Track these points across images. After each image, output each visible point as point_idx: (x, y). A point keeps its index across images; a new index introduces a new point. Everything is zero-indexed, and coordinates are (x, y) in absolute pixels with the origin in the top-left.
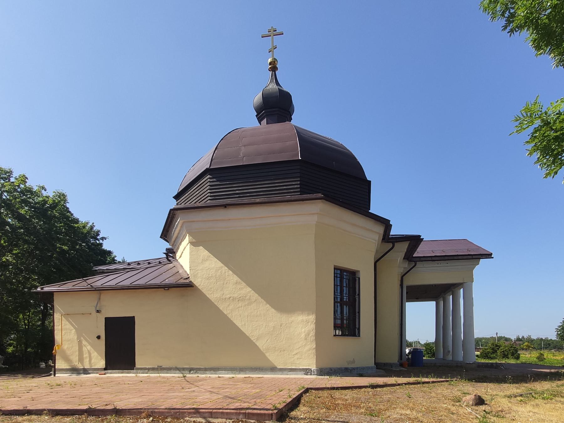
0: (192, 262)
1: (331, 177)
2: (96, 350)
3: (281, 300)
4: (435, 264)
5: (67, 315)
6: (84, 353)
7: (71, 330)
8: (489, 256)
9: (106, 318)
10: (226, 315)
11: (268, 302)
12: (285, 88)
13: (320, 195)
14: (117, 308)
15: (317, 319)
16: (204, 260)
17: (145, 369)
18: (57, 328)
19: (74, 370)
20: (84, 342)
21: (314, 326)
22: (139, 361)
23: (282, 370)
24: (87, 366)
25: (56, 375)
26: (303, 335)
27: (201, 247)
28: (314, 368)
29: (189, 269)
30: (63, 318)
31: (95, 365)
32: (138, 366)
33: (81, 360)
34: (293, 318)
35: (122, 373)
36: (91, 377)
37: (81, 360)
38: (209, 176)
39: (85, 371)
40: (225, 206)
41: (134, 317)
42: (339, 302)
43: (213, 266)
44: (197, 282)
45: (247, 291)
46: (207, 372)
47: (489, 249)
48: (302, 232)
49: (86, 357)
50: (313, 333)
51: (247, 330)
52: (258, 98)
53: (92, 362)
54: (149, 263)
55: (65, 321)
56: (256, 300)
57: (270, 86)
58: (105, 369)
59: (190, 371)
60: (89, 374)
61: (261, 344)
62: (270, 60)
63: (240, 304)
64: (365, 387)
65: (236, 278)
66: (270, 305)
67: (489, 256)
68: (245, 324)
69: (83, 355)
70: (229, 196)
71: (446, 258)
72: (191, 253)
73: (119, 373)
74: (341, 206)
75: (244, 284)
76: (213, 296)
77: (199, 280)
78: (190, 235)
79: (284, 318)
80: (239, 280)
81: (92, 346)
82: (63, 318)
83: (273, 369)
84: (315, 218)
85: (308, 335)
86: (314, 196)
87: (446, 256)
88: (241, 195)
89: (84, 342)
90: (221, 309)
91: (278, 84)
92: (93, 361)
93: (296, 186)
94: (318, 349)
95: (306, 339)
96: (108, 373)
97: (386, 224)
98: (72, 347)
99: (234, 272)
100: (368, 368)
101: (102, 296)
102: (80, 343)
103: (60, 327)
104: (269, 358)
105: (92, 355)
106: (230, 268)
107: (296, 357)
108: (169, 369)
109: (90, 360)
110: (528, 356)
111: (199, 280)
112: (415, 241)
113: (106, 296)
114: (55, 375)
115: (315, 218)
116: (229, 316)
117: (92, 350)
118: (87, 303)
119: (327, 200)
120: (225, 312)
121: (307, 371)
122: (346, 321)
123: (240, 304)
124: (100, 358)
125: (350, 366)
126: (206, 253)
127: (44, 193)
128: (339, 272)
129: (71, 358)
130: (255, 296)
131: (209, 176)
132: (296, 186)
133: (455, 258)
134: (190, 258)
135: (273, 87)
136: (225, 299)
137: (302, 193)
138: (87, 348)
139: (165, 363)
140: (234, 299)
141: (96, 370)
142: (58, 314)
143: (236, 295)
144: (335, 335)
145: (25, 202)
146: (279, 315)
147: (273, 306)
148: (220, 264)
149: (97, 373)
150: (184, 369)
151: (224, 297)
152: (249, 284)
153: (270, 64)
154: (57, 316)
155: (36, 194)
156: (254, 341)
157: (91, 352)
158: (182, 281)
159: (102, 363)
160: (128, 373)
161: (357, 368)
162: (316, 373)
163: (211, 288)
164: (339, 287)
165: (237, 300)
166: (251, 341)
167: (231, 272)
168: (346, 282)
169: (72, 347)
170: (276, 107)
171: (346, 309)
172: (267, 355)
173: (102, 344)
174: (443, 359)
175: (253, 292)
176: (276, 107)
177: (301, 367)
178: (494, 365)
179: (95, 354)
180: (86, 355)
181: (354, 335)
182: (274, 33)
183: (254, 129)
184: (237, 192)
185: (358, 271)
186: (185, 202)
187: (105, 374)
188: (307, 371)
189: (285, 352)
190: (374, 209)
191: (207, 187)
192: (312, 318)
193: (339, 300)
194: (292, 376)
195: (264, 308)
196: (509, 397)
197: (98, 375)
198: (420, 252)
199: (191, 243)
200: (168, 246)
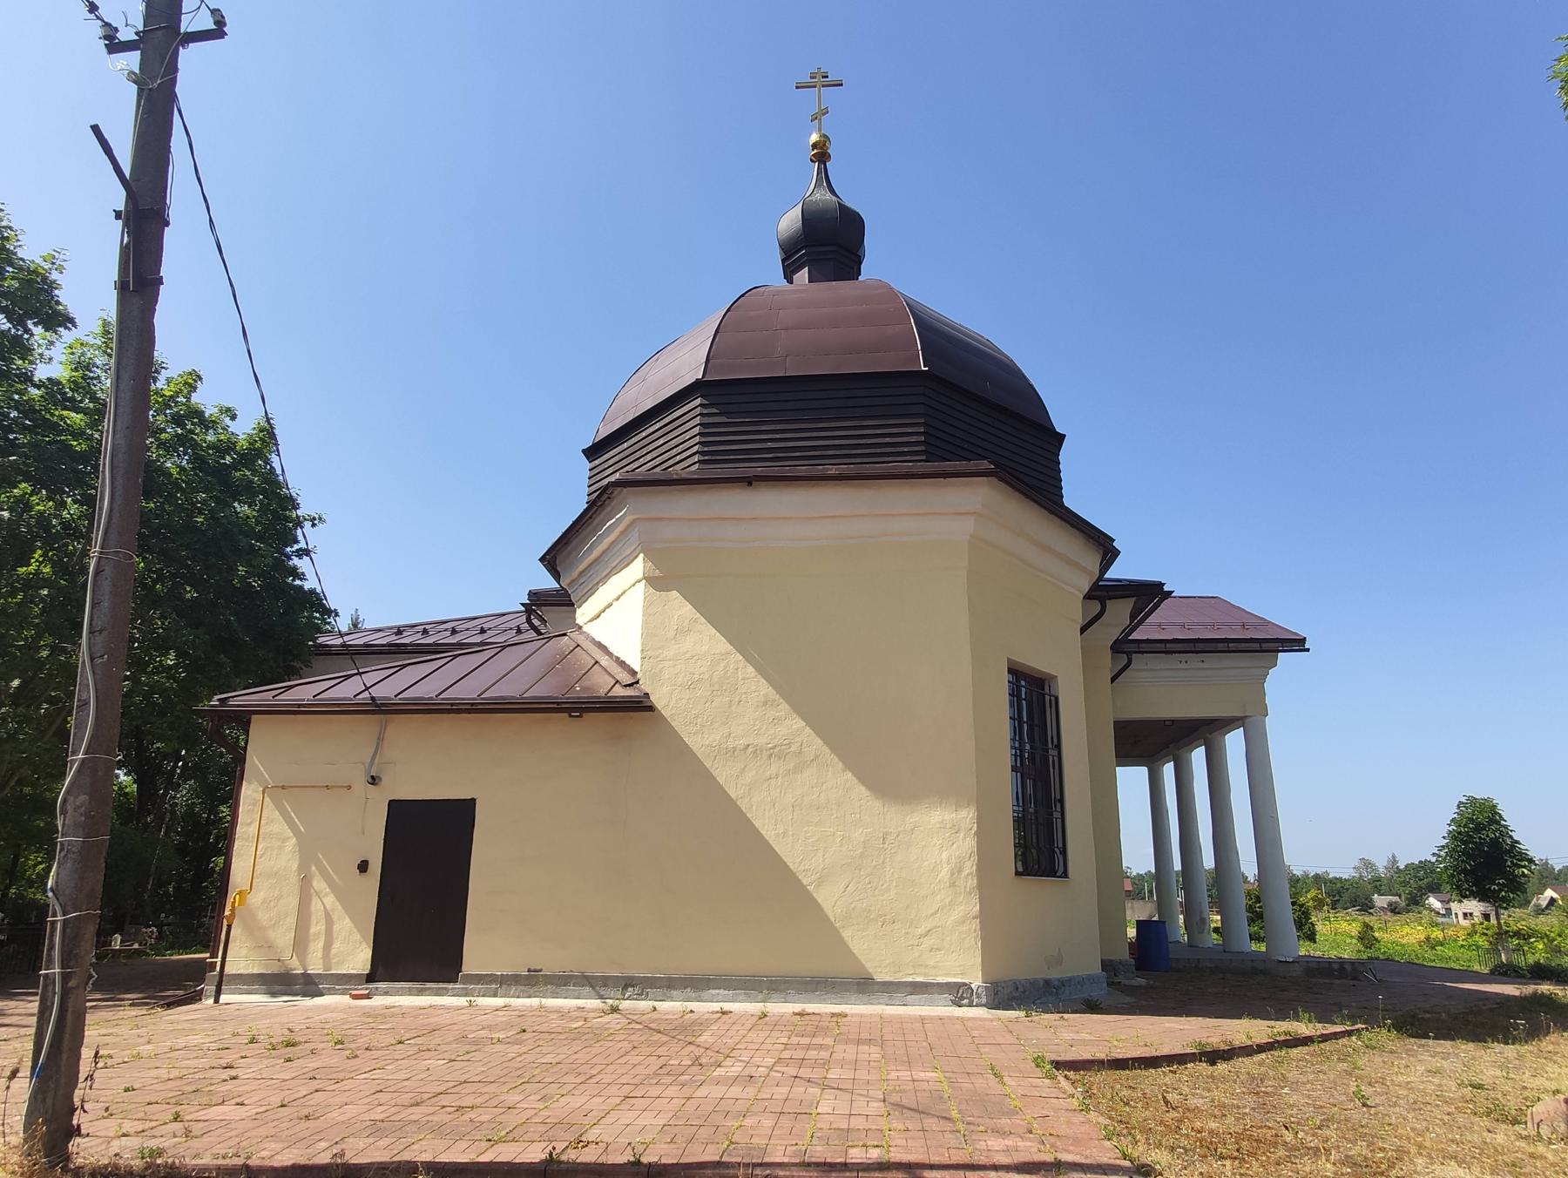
0: (649, 635)
1: (967, 419)
2: (349, 909)
4: (1172, 661)
5: (279, 790)
6: (314, 919)
7: (284, 841)
8: (1297, 644)
9: (392, 803)
10: (733, 803)
11: (849, 765)
12: (850, 203)
13: (985, 465)
14: (427, 770)
15: (980, 820)
16: (681, 632)
17: (491, 979)
18: (245, 831)
19: (282, 983)
21: (974, 843)
22: (477, 953)
24: (315, 968)
25: (224, 998)
26: (944, 873)
28: (976, 981)
29: (639, 655)
30: (267, 799)
32: (470, 965)
33: (300, 943)
34: (915, 818)
35: (420, 992)
36: (325, 1008)
37: (300, 943)
38: (698, 401)
39: (309, 985)
40: (749, 481)
41: (470, 804)
43: (705, 648)
45: (794, 726)
46: (675, 993)
47: (1296, 627)
48: (915, 557)
50: (970, 867)
51: (789, 852)
52: (790, 221)
53: (333, 952)
54: (483, 631)
55: (271, 811)
56: (817, 757)
57: (818, 196)
58: (370, 978)
59: (625, 988)
60: (322, 995)
61: (830, 899)
62: (814, 138)
63: (773, 770)
64: (1180, 1059)
65: (764, 689)
66: (854, 774)
67: (1297, 644)
69: (308, 928)
70: (749, 456)
71: (1200, 646)
73: (410, 992)
74: (1027, 496)
75: (785, 706)
76: (700, 741)
77: (666, 689)
78: (649, 556)
79: (893, 818)
81: (340, 897)
82: (267, 799)
83: (865, 986)
84: (969, 525)
85: (960, 871)
86: (972, 465)
87: (1199, 640)
88: (780, 455)
89: (319, 884)
92: (337, 947)
93: (914, 439)
94: (985, 917)
95: (953, 885)
96: (377, 992)
97: (1107, 550)
98: (280, 897)
99: (761, 671)
100: (1082, 981)
102: (305, 881)
103: (253, 829)
104: (851, 945)
105: (336, 928)
106: (749, 659)
107: (927, 943)
108: (560, 982)
110: (1337, 936)
111: (666, 689)
112: (1149, 594)
113: (401, 730)
114: (216, 1001)
115: (969, 525)
117: (338, 910)
118: (338, 751)
119: (1001, 480)
121: (959, 993)
123: (773, 770)
124: (358, 937)
125: (1055, 974)
127: (234, 427)
129: (271, 934)
130: (813, 743)
131: (698, 401)
132: (914, 439)
133: (1221, 646)
134: (645, 623)
136: (734, 749)
137: (931, 456)
138: (325, 900)
139: (552, 962)
142: (255, 785)
143: (762, 740)
145: (184, 440)
146: (877, 805)
147: (863, 779)
148: (723, 645)
149: (344, 993)
150: (606, 982)
151: (731, 745)
152: (799, 709)
153: (814, 146)
154: (249, 792)
155: (207, 424)
156: (810, 888)
157: (335, 918)
158: (619, 691)
159: (359, 958)
160: (438, 993)
161: (1070, 980)
162: (984, 1000)
163: (697, 717)
165: (765, 755)
166: (802, 888)
167: (751, 669)
169: (280, 897)
170: (828, 243)
174: (1190, 945)
175: (808, 730)
176: (828, 243)
177: (941, 980)
178: (1348, 967)
179: (344, 924)
180: (317, 928)
182: (823, 81)
183: (777, 293)
184: (770, 445)
185: (1055, 677)
186: (615, 467)
187: (368, 997)
188: (959, 993)
189: (896, 926)
191: (693, 428)
192: (966, 817)
194: (917, 1009)
195: (836, 782)
196: (1474, 1087)
197: (346, 999)
198: (1159, 625)
199: (650, 580)
200: (547, 582)
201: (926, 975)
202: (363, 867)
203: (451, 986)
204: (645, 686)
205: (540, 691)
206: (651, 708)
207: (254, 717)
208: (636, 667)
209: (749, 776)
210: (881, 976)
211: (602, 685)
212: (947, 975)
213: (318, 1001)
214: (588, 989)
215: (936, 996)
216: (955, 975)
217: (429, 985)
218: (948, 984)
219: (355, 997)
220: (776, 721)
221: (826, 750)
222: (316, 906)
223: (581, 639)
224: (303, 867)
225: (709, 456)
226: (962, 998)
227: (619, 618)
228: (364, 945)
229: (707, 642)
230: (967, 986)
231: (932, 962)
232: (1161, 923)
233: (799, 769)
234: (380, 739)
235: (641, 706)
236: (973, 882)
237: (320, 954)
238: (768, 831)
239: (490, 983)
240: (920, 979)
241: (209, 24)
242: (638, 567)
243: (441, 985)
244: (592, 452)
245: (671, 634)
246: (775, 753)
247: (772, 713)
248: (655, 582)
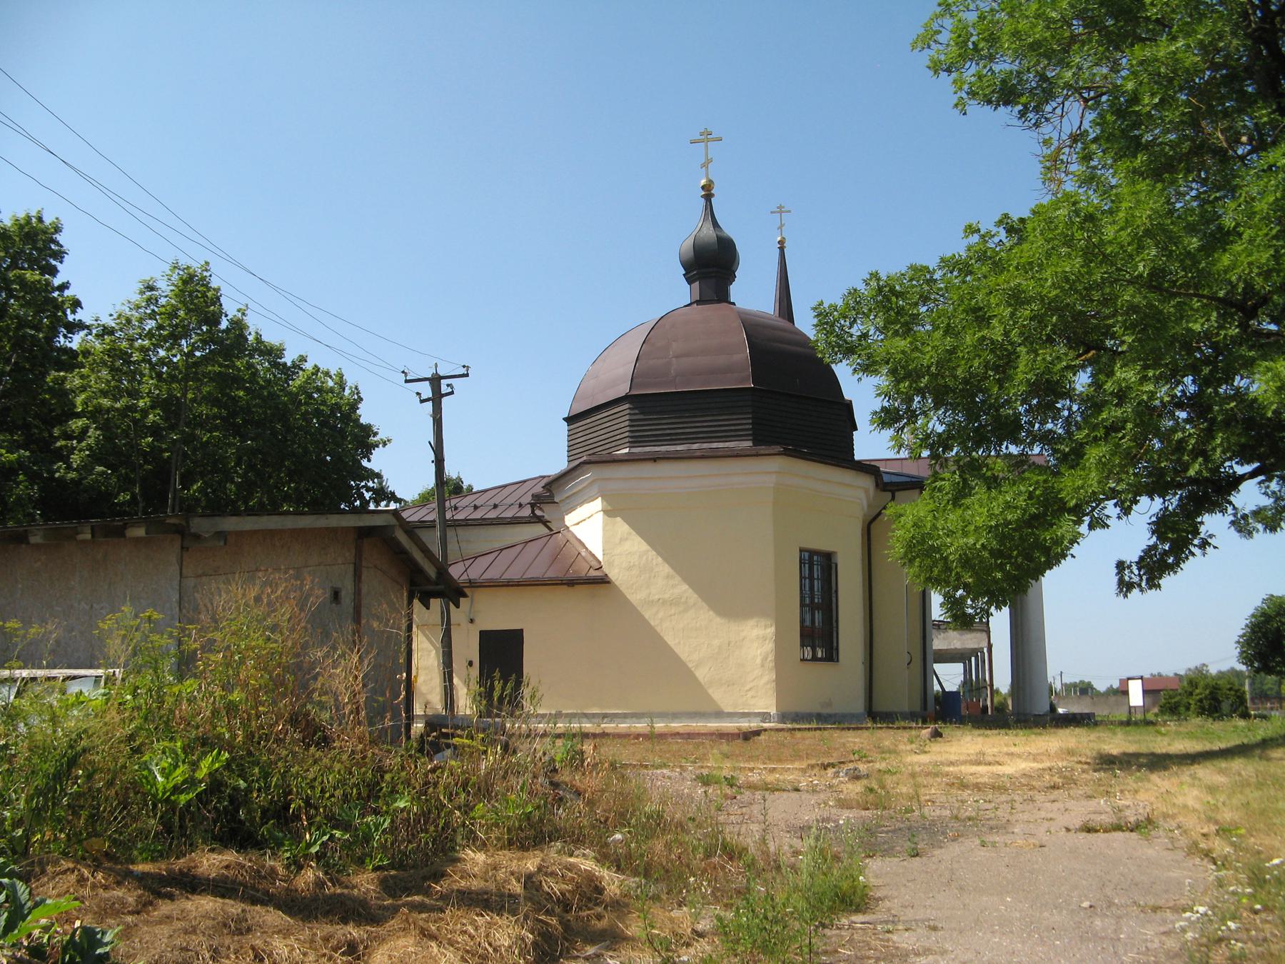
0: (606, 541)
3: (726, 601)
12: (729, 230)
16: (622, 540)
23: (731, 715)
26: (758, 661)
27: (619, 519)
28: (773, 711)
40: (655, 459)
42: (807, 605)
44: (613, 574)
45: (683, 589)
48: (758, 497)
50: (771, 657)
61: (702, 674)
62: (703, 182)
65: (667, 569)
72: (605, 525)
75: (678, 578)
76: (635, 597)
80: (671, 572)
83: (719, 714)
91: (715, 224)
99: (666, 560)
106: (659, 553)
107: (750, 694)
116: (658, 629)
120: (652, 623)
122: (817, 634)
125: (825, 711)
126: (626, 528)
128: (807, 555)
130: (693, 597)
135: (709, 233)
140: (664, 602)
143: (667, 596)
144: (803, 660)
146: (718, 620)
148: (644, 546)
152: (687, 579)
153: (703, 188)
158: (593, 573)
168: (818, 571)
170: (712, 266)
171: (818, 616)
172: (710, 691)
176: (712, 266)
181: (812, 553)
182: (707, 137)
185: (835, 553)
190: (860, 454)
191: (624, 422)
193: (807, 601)
195: (704, 616)
199: (605, 511)
202: (471, 664)
204: (606, 569)
205: (550, 574)
206: (609, 582)
208: (600, 558)
209: (661, 615)
211: (583, 570)
220: (673, 586)
223: (569, 536)
227: (589, 525)
229: (636, 545)
235: (604, 581)
236: (772, 664)
238: (670, 640)
241: (464, 371)
242: (597, 504)
244: (570, 420)
246: (674, 602)
248: (608, 513)
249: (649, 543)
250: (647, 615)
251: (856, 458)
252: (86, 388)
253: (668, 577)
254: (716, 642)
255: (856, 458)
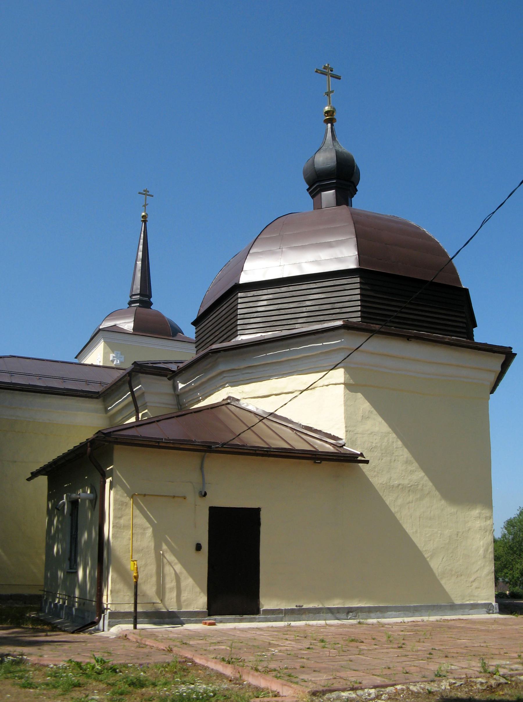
7: (145, 529)
14: (233, 489)
16: (365, 418)
20: (170, 557)
23: (463, 607)
24: (173, 608)
25: (139, 626)
26: (481, 551)
27: (359, 395)
31: (187, 605)
35: (241, 621)
39: (172, 618)
41: (256, 512)
49: (171, 589)
51: (419, 540)
59: (348, 613)
60: (182, 624)
61: (436, 565)
63: (410, 498)
68: (416, 532)
75: (416, 464)
81: (184, 565)
83: (453, 607)
85: (487, 550)
90: (388, 502)
92: (184, 596)
93: (461, 325)
95: (484, 557)
99: (406, 444)
101: (207, 463)
104: (445, 587)
107: (475, 585)
109: (454, 653)
114: (135, 627)
116: (398, 516)
121: (488, 608)
123: (410, 498)
124: (198, 589)
132: (461, 325)
134: (346, 411)
136: (393, 486)
138: (174, 567)
141: (194, 616)
143: (406, 482)
146: (451, 509)
152: (424, 467)
153: (327, 112)
156: (428, 559)
157: (182, 578)
159: (200, 601)
160: (251, 621)
162: (498, 610)
164: (254, 452)
166: (424, 559)
172: (443, 582)
173: (202, 560)
175: (426, 478)
177: (480, 602)
179: (188, 582)
180: (170, 584)
187: (214, 624)
188: (488, 608)
189: (463, 577)
195: (436, 505)
199: (347, 385)
201: (474, 600)
203: (257, 616)
207: (116, 447)
209: (400, 501)
210: (458, 602)
212: (482, 600)
213: (180, 628)
214: (330, 615)
215: (481, 610)
216: (485, 600)
217: (245, 616)
218: (485, 604)
219: (210, 624)
220: (412, 472)
221: (434, 488)
222: (168, 569)
224: (158, 547)
225: (365, 314)
226: (490, 610)
228: (202, 594)
230: (491, 604)
231: (476, 594)
232: (256, 611)
233: (421, 499)
234: (202, 468)
237: (175, 600)
239: (279, 613)
240: (472, 602)
243: (252, 616)
245: (360, 419)
246: (411, 489)
247: (410, 468)
249: (390, 425)
250: (389, 499)
251: (474, 329)
252: (359, 267)
253: (407, 462)
254: (447, 532)
255: (474, 329)
